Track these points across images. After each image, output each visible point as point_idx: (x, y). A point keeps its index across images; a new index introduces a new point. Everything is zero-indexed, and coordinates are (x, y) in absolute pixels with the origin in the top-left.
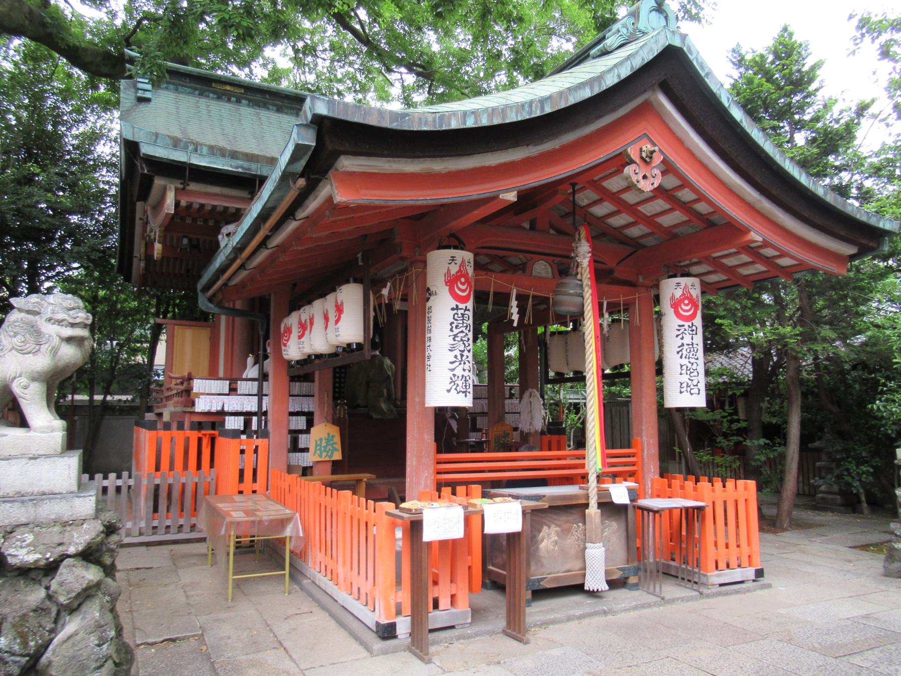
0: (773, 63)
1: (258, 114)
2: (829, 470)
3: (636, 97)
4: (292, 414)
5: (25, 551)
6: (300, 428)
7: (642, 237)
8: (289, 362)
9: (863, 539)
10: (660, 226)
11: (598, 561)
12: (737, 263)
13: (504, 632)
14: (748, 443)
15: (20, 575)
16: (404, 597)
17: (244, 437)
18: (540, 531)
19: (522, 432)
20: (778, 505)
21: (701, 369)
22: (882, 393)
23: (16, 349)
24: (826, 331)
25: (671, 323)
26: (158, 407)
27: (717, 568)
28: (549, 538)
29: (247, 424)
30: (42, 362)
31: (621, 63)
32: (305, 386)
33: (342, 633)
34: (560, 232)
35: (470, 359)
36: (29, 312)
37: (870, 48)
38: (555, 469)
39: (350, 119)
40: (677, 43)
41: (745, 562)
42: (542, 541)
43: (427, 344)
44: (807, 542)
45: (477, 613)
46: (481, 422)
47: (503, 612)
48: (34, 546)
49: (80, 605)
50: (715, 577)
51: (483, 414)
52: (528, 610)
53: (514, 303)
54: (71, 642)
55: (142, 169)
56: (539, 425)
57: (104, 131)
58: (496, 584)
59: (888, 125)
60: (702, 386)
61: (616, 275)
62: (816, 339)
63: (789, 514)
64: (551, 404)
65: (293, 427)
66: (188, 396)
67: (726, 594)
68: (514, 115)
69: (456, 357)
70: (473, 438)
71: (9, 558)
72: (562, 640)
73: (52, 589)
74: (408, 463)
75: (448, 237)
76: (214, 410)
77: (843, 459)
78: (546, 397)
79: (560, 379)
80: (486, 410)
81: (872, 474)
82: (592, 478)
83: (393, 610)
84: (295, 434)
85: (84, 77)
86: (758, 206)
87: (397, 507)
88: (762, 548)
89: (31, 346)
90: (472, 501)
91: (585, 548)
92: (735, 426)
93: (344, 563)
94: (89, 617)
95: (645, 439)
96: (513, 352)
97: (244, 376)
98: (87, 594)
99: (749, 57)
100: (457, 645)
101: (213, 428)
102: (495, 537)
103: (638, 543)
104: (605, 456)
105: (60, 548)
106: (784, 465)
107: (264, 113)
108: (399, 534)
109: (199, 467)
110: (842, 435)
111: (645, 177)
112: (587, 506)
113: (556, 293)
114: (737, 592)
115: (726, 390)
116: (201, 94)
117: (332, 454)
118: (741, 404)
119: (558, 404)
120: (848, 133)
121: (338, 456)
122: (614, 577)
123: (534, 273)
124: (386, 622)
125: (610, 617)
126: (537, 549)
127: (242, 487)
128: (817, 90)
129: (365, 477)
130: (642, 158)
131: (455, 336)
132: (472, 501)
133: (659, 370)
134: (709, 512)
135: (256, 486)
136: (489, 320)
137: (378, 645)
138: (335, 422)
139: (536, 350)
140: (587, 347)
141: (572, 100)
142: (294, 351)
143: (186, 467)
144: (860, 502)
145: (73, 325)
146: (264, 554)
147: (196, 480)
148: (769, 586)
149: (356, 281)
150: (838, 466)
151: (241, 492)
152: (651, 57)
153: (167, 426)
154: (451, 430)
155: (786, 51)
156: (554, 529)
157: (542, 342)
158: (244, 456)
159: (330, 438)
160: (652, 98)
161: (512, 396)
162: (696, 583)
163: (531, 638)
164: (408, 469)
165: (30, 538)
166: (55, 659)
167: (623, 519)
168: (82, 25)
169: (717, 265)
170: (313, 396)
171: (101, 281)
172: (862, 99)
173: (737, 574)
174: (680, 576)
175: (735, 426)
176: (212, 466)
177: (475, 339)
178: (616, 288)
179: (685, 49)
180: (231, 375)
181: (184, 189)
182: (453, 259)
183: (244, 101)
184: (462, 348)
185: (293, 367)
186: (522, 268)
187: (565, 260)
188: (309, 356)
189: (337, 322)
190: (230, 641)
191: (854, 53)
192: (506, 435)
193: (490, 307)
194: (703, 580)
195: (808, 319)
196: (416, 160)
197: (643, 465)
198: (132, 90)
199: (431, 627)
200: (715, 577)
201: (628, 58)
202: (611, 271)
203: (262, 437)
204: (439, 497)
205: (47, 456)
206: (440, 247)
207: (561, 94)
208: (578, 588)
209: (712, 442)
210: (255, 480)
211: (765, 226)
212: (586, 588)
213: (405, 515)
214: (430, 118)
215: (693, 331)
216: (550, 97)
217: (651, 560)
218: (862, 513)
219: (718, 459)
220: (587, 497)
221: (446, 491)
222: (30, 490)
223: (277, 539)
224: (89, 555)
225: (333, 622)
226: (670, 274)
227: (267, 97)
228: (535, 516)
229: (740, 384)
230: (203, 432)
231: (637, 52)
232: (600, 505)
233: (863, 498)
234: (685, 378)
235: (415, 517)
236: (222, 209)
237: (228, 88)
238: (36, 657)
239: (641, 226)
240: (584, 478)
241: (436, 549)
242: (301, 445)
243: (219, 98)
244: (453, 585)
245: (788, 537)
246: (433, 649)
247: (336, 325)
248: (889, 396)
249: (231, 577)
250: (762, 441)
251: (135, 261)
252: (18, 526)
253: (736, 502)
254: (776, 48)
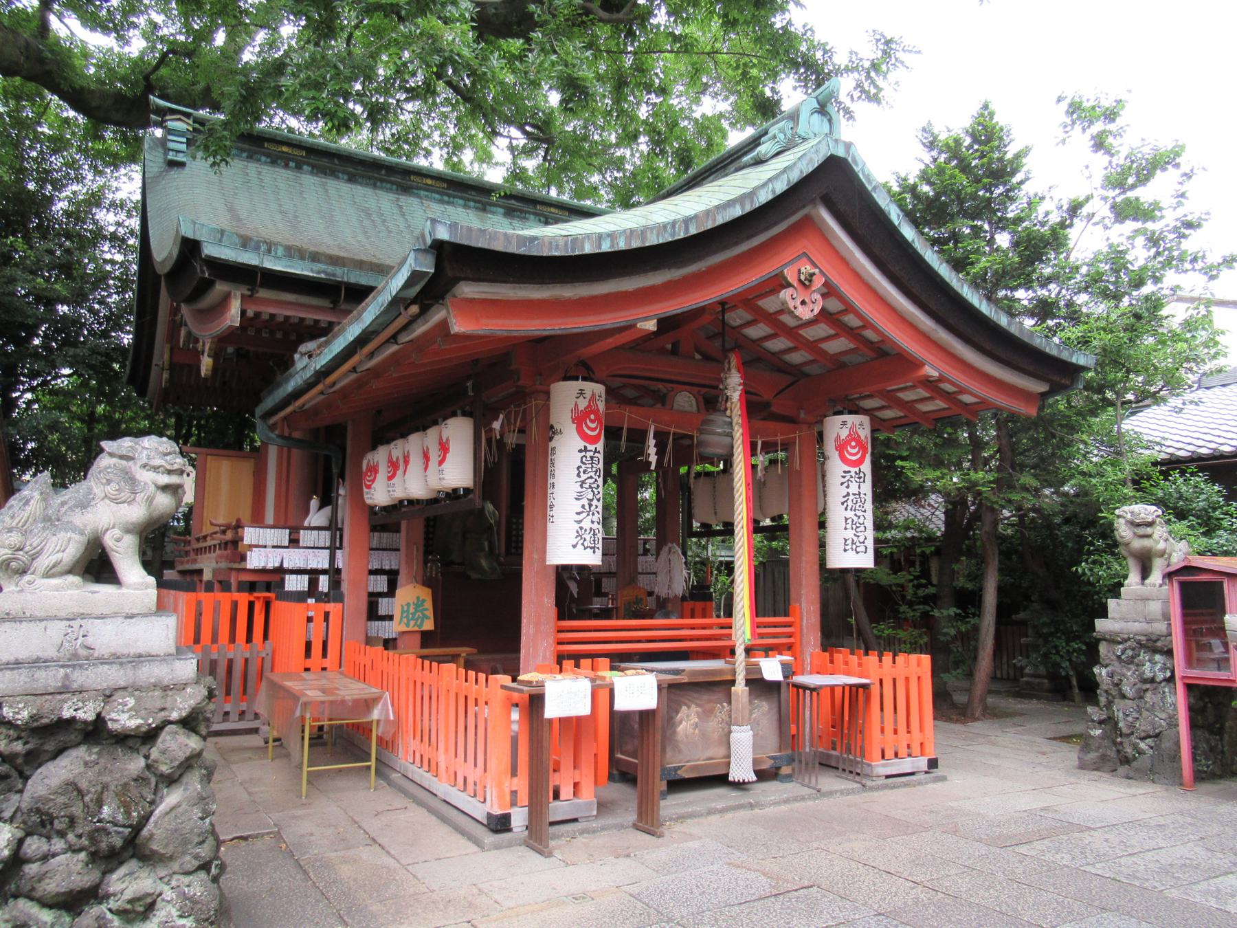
0: (969, 147)
1: (324, 184)
2: (1036, 648)
3: (793, 213)
4: (372, 572)
5: (126, 716)
6: (380, 590)
7: (805, 364)
8: (372, 508)
9: (1066, 729)
10: (824, 353)
11: (744, 749)
12: (914, 398)
13: (636, 827)
14: (936, 613)
15: (117, 743)
16: (521, 784)
17: (311, 601)
18: (677, 712)
19: (658, 597)
20: (969, 691)
21: (869, 523)
22: (1090, 553)
23: (110, 499)
24: (1027, 479)
25: (836, 468)
26: (182, 563)
27: (883, 757)
28: (688, 720)
29: (313, 583)
30: (136, 513)
31: (776, 177)
32: (387, 538)
33: (445, 830)
34: (707, 357)
35: (600, 509)
36: (121, 457)
37: (1081, 139)
38: (698, 640)
39: (473, 244)
40: (841, 152)
41: (916, 749)
42: (680, 723)
43: (550, 491)
44: (999, 733)
45: (603, 807)
46: (608, 585)
47: (634, 805)
48: (136, 711)
49: (181, 776)
50: (881, 768)
51: (609, 574)
52: (662, 803)
53: (652, 442)
54: (173, 814)
55: (203, 272)
56: (679, 588)
57: (117, 198)
58: (624, 775)
59: (1106, 228)
60: (870, 543)
61: (774, 409)
62: (1014, 487)
63: (983, 700)
64: (696, 563)
65: (371, 589)
66: (234, 548)
67: (894, 787)
68: (655, 236)
69: (583, 506)
70: (597, 604)
71: (110, 724)
72: (702, 846)
73: (152, 757)
74: (524, 631)
75: (576, 365)
76: (270, 566)
77: (1052, 634)
78: (689, 553)
79: (707, 531)
80: (614, 569)
81: (1083, 652)
82: (740, 651)
83: (508, 798)
84: (373, 598)
85: (81, 119)
86: (934, 336)
87: (514, 680)
88: (931, 733)
89: (125, 495)
90: (600, 673)
91: (730, 732)
92: (921, 592)
93: (447, 750)
94: (191, 788)
95: (804, 606)
96: (648, 494)
97: (306, 524)
98: (188, 764)
99: (942, 137)
100: (581, 839)
101: (268, 589)
102: (627, 715)
103: (793, 730)
104: (755, 626)
105: (163, 714)
106: (977, 640)
107: (332, 184)
108: (515, 715)
109: (249, 639)
110: (1051, 605)
111: (803, 303)
112: (733, 682)
113: (701, 432)
114: (906, 785)
115: (912, 547)
116: (250, 157)
117: (422, 622)
118: (934, 566)
119: (704, 562)
120: (1055, 239)
121: (429, 625)
122: (764, 767)
123: (675, 406)
124: (499, 812)
125: (757, 811)
126: (675, 732)
127: (309, 663)
128: (1022, 182)
129: (464, 651)
130: (800, 280)
131: (583, 482)
132: (600, 673)
133: (822, 525)
134: (875, 690)
135: (327, 663)
136: (622, 464)
137: (490, 838)
138: (427, 583)
139: (677, 493)
140: (736, 496)
141: (720, 220)
142: (380, 494)
143: (232, 639)
144: (1071, 687)
145: (170, 472)
146: (345, 743)
147: (247, 655)
148: (944, 779)
149: (465, 414)
150: (1046, 641)
151: (307, 670)
152: (811, 170)
153: (209, 587)
154: (577, 593)
155: (986, 133)
156: (694, 709)
157: (684, 487)
158: (311, 625)
159: (419, 603)
160: (813, 212)
161: (646, 552)
162: (858, 774)
163: (666, 833)
164: (523, 639)
165: (131, 702)
166: (157, 832)
167: (776, 698)
168: (86, 55)
169: (892, 399)
170: (398, 550)
171: (99, 393)
172: (1072, 197)
173: (906, 765)
174: (841, 767)
175: (921, 592)
176: (266, 637)
177: (605, 482)
178: (771, 425)
179: (849, 159)
180: (286, 521)
181: (250, 296)
182: (581, 392)
183: (305, 167)
184: (590, 496)
185: (376, 514)
186: (662, 399)
187: (713, 392)
188: (401, 502)
189: (441, 463)
190: (313, 838)
191: (1064, 141)
192: (638, 601)
193: (623, 443)
194: (867, 770)
195: (1011, 459)
196: (545, 286)
197: (802, 636)
198: (161, 150)
199: (552, 819)
200: (881, 768)
201: (785, 170)
202: (767, 405)
203: (335, 600)
204: (561, 671)
205: (145, 615)
206: (566, 378)
207: (707, 213)
208: (721, 780)
209: (896, 613)
210: (324, 655)
211: (939, 357)
212: (731, 779)
213: (526, 688)
214: (561, 242)
216: (696, 216)
217: (807, 750)
218: (1073, 700)
219: (902, 634)
220: (734, 672)
221: (568, 664)
222: (126, 651)
223: (353, 724)
224: (189, 723)
225: (434, 818)
226: (836, 409)
227: (336, 161)
228: (672, 691)
229: (930, 539)
230: (256, 594)
231: (794, 164)
232: (749, 682)
233: (1074, 682)
234: (850, 534)
235: (534, 691)
236: (296, 321)
237: (285, 149)
238: (137, 829)
239: (802, 352)
240: (732, 652)
241: (556, 725)
242: (382, 612)
243: (273, 162)
244: (577, 772)
245: (978, 727)
246: (552, 843)
247: (438, 465)
248: (1096, 557)
249: (306, 769)
250: (953, 611)
251: (154, 371)
252: (116, 690)
253: (907, 679)
254: (973, 129)
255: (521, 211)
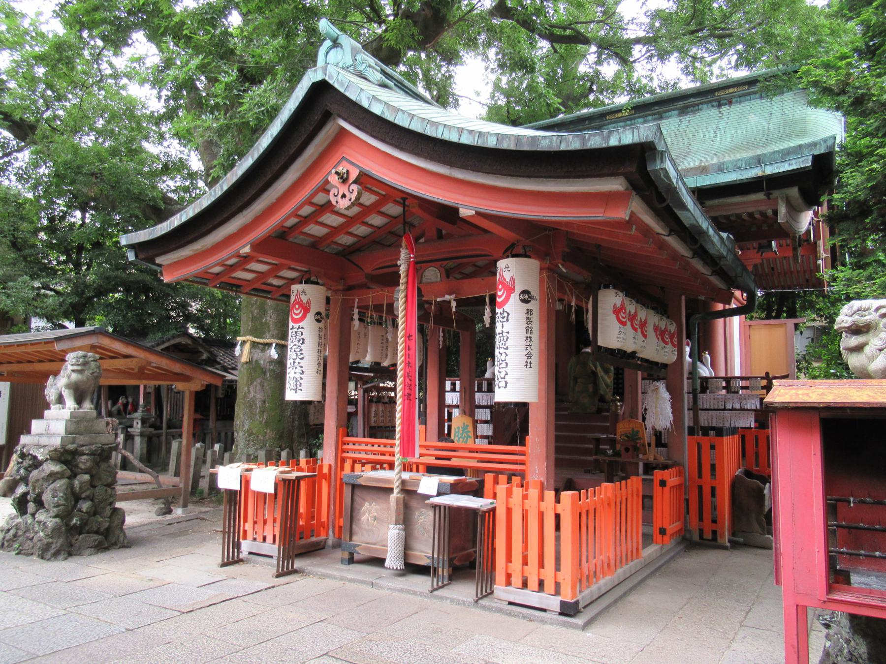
38: (501, 463)
50: (501, 590)
53: (356, 311)
134: (501, 514)
173: (531, 597)
184: (295, 357)
215: (503, 318)
255: (693, 106)
